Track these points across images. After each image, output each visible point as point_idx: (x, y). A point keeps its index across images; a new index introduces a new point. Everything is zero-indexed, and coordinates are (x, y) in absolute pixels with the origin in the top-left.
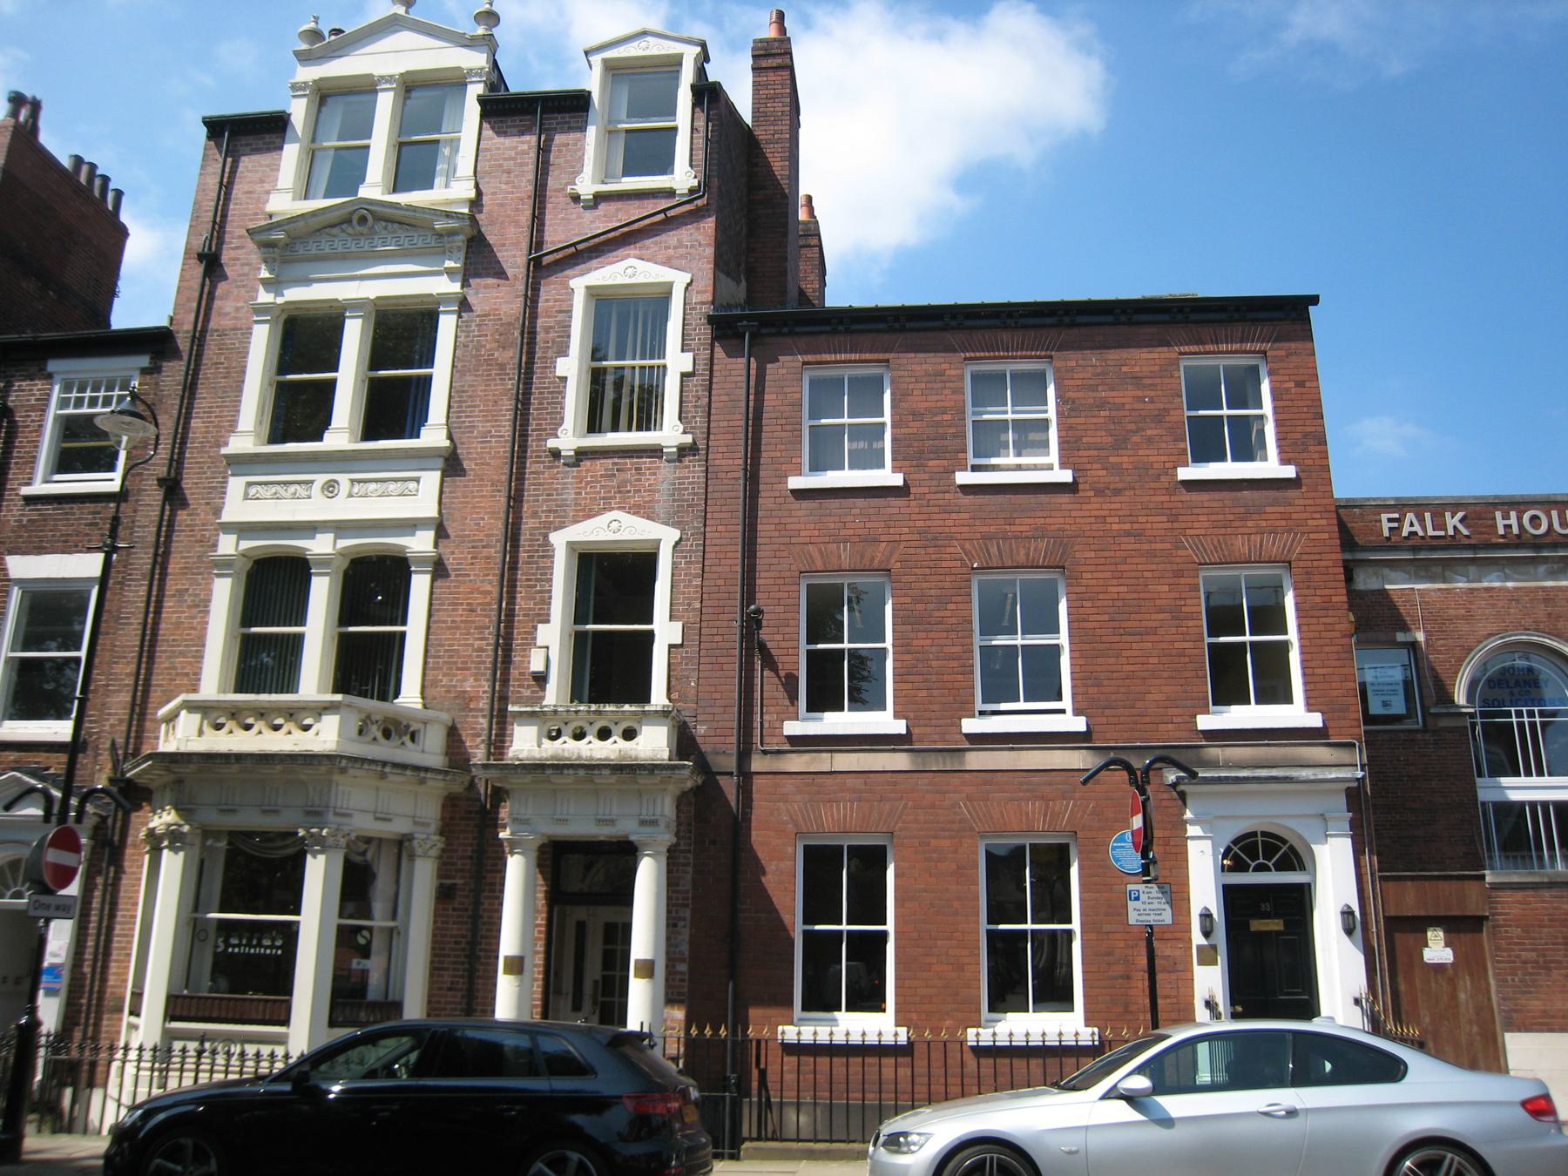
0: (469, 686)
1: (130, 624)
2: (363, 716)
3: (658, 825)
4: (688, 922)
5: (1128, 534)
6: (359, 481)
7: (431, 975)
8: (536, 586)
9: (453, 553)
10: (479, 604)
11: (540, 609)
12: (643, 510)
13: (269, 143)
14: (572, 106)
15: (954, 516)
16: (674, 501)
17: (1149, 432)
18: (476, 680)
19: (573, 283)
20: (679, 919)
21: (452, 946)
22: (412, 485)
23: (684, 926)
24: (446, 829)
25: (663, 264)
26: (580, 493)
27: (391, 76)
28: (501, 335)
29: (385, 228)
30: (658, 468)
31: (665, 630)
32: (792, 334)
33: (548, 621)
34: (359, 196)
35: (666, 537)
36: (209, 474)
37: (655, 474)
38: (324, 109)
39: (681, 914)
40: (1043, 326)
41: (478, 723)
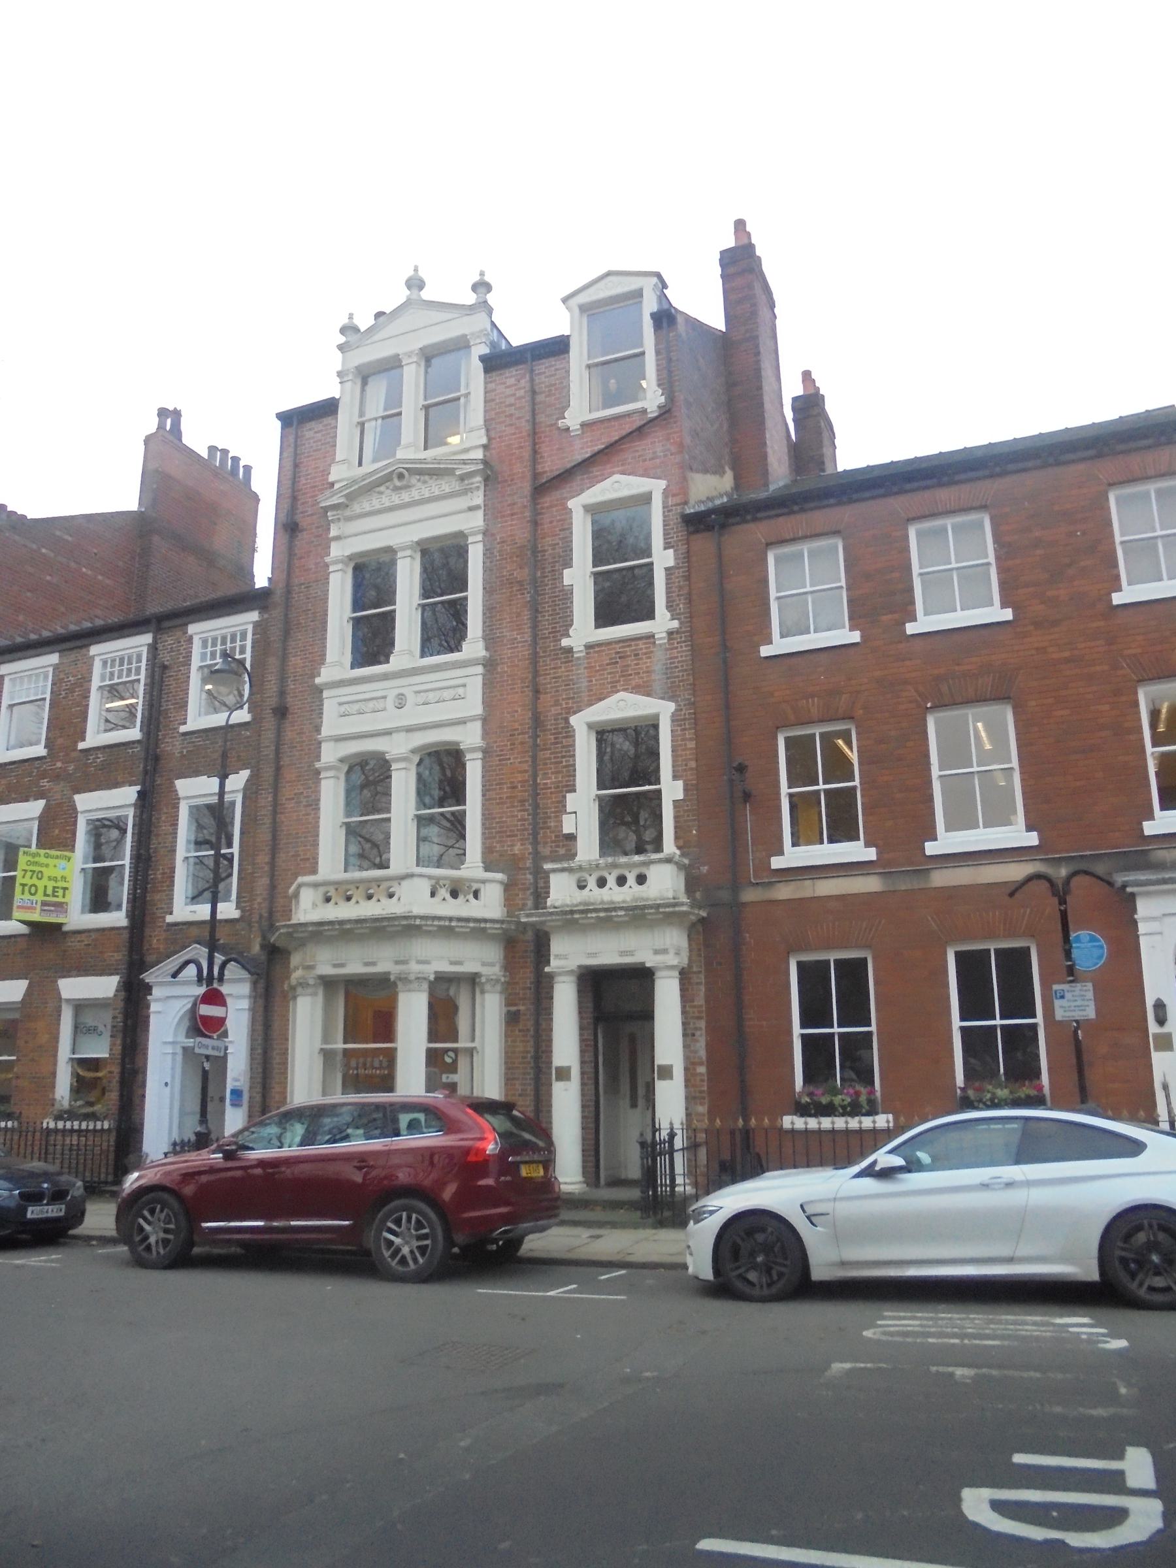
0: (517, 849)
1: (264, 824)
2: (433, 882)
3: (668, 953)
4: (704, 1032)
5: (1067, 660)
6: (419, 692)
7: (506, 1084)
8: (562, 762)
9: (496, 742)
10: (520, 782)
11: (567, 781)
12: (645, 689)
13: (326, 425)
14: (557, 347)
15: (908, 663)
16: (668, 678)
17: (1082, 564)
18: (522, 845)
19: (571, 504)
20: (696, 1029)
21: (520, 1060)
22: (461, 691)
23: (701, 1035)
24: (510, 965)
25: (642, 476)
26: (591, 681)
27: (412, 352)
28: (517, 557)
29: (419, 480)
30: (652, 652)
31: (671, 790)
32: (755, 520)
33: (575, 791)
34: (398, 457)
35: (664, 710)
36: (309, 700)
37: (650, 658)
38: (368, 388)
39: (698, 1025)
40: (978, 479)
41: (526, 879)
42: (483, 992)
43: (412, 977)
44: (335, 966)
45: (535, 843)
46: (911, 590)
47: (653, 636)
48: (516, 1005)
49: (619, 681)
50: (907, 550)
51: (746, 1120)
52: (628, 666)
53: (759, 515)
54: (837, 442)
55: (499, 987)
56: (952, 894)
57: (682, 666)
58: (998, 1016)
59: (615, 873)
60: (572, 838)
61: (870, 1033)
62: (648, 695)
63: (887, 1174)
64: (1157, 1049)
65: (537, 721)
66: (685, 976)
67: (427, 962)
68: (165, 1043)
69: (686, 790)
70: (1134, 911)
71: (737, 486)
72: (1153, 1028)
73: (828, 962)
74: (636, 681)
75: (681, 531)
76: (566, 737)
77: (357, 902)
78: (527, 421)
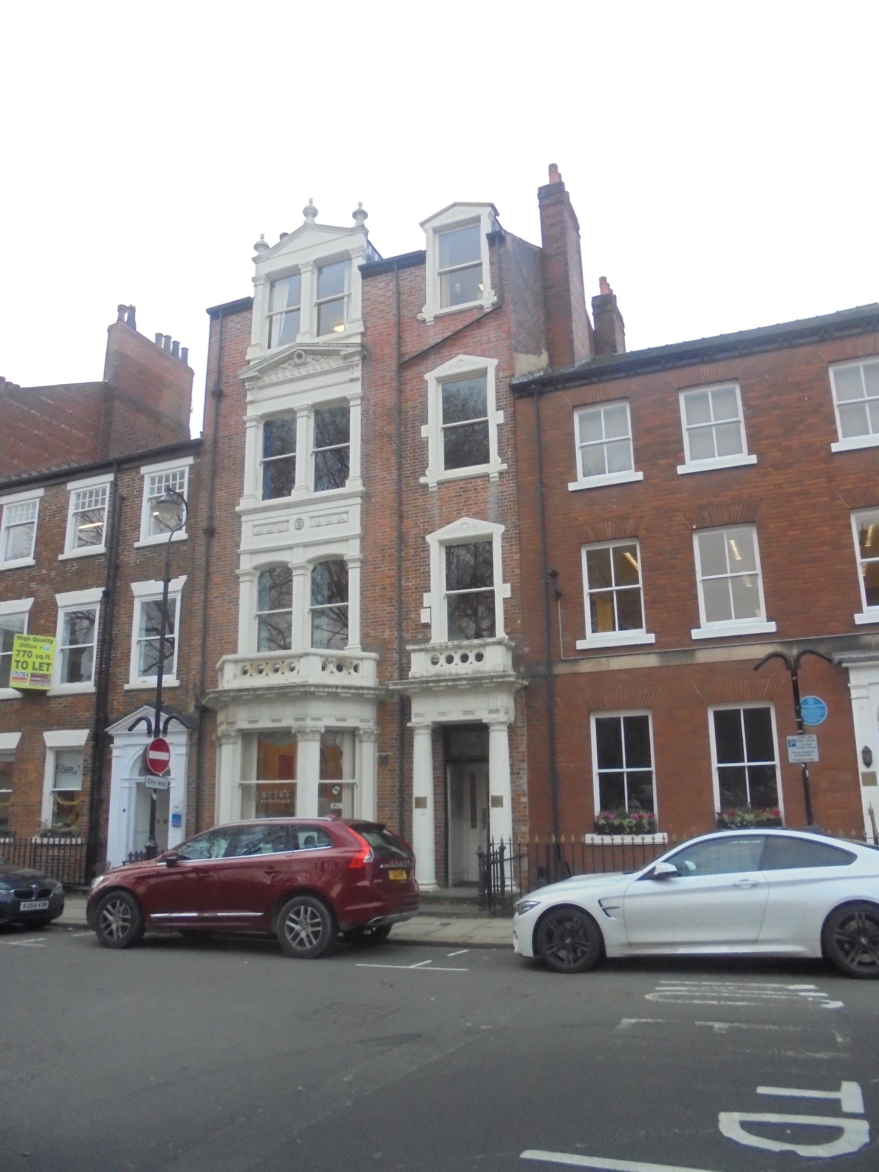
0: (386, 635)
1: (198, 616)
2: (324, 659)
3: (499, 712)
4: (526, 771)
5: (798, 494)
6: (313, 517)
7: (378, 810)
8: (420, 570)
9: (371, 555)
10: (389, 584)
11: (424, 584)
12: (482, 515)
13: (244, 318)
14: (416, 260)
15: (678, 495)
16: (499, 507)
17: (809, 421)
18: (390, 631)
19: (427, 377)
20: (520, 769)
21: (389, 792)
22: (344, 516)
23: (524, 774)
24: (381, 721)
25: (480, 356)
26: (442, 509)
27: (308, 263)
28: (386, 416)
29: (313, 359)
30: (487, 487)
31: (502, 590)
32: (564, 388)
33: (430, 591)
34: (297, 342)
35: (496, 531)
36: (231, 523)
37: (486, 492)
38: (275, 290)
39: (521, 766)
40: (731, 358)
41: (393, 657)
42: (361, 742)
43: (308, 730)
44: (251, 722)
45: (400, 630)
46: (681, 441)
47: (488, 475)
48: (385, 751)
49: (462, 509)
50: (678, 411)
51: (558, 837)
52: (470, 498)
53: (567, 385)
54: (625, 330)
55: (373, 738)
56: (711, 668)
57: (510, 498)
58: (746, 759)
59: (460, 653)
60: (427, 626)
61: (650, 772)
62: (485, 519)
63: (663, 877)
64: (865, 784)
65: (402, 539)
66: (512, 730)
67: (319, 719)
68: (124, 780)
69: (513, 590)
70: (848, 681)
71: (551, 363)
72: (862, 768)
73: (619, 719)
74: (475, 509)
75: (509, 397)
76: (423, 551)
77: (267, 674)
78: (394, 315)
